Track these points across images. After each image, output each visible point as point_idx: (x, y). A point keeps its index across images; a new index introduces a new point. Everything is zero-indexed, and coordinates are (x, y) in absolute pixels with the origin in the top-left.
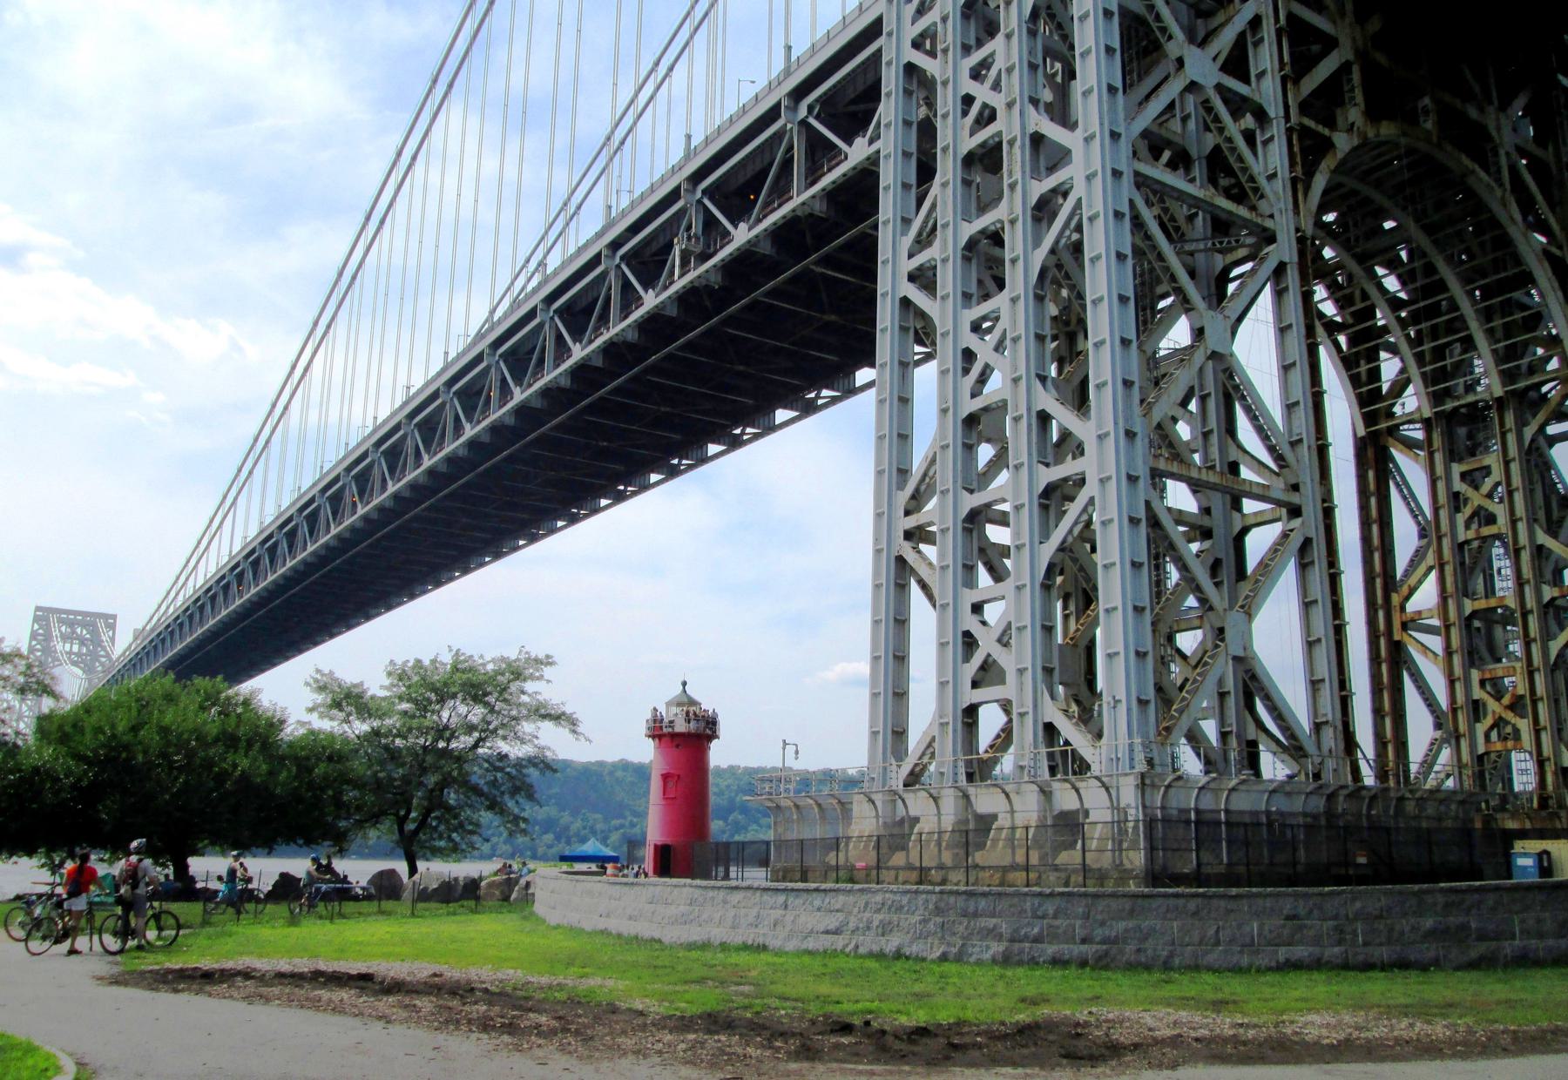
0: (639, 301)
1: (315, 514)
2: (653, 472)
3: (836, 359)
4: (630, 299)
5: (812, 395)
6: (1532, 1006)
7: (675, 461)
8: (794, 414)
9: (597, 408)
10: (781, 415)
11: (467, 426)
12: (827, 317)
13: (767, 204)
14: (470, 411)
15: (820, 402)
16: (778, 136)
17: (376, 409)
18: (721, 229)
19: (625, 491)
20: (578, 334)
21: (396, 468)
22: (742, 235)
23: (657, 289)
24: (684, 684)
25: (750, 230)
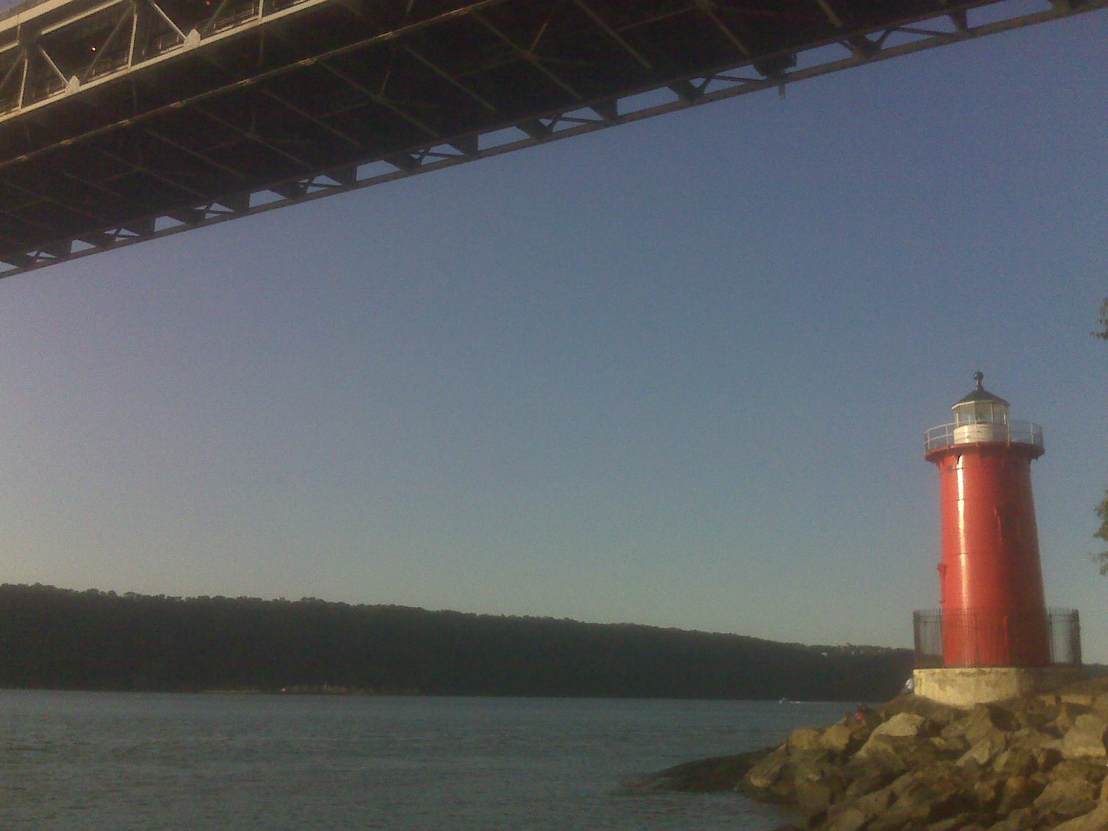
2: (258, 187)
4: (42, 83)
5: (112, 232)
10: (77, 245)
23: (205, 29)
24: (980, 376)
25: (202, 38)
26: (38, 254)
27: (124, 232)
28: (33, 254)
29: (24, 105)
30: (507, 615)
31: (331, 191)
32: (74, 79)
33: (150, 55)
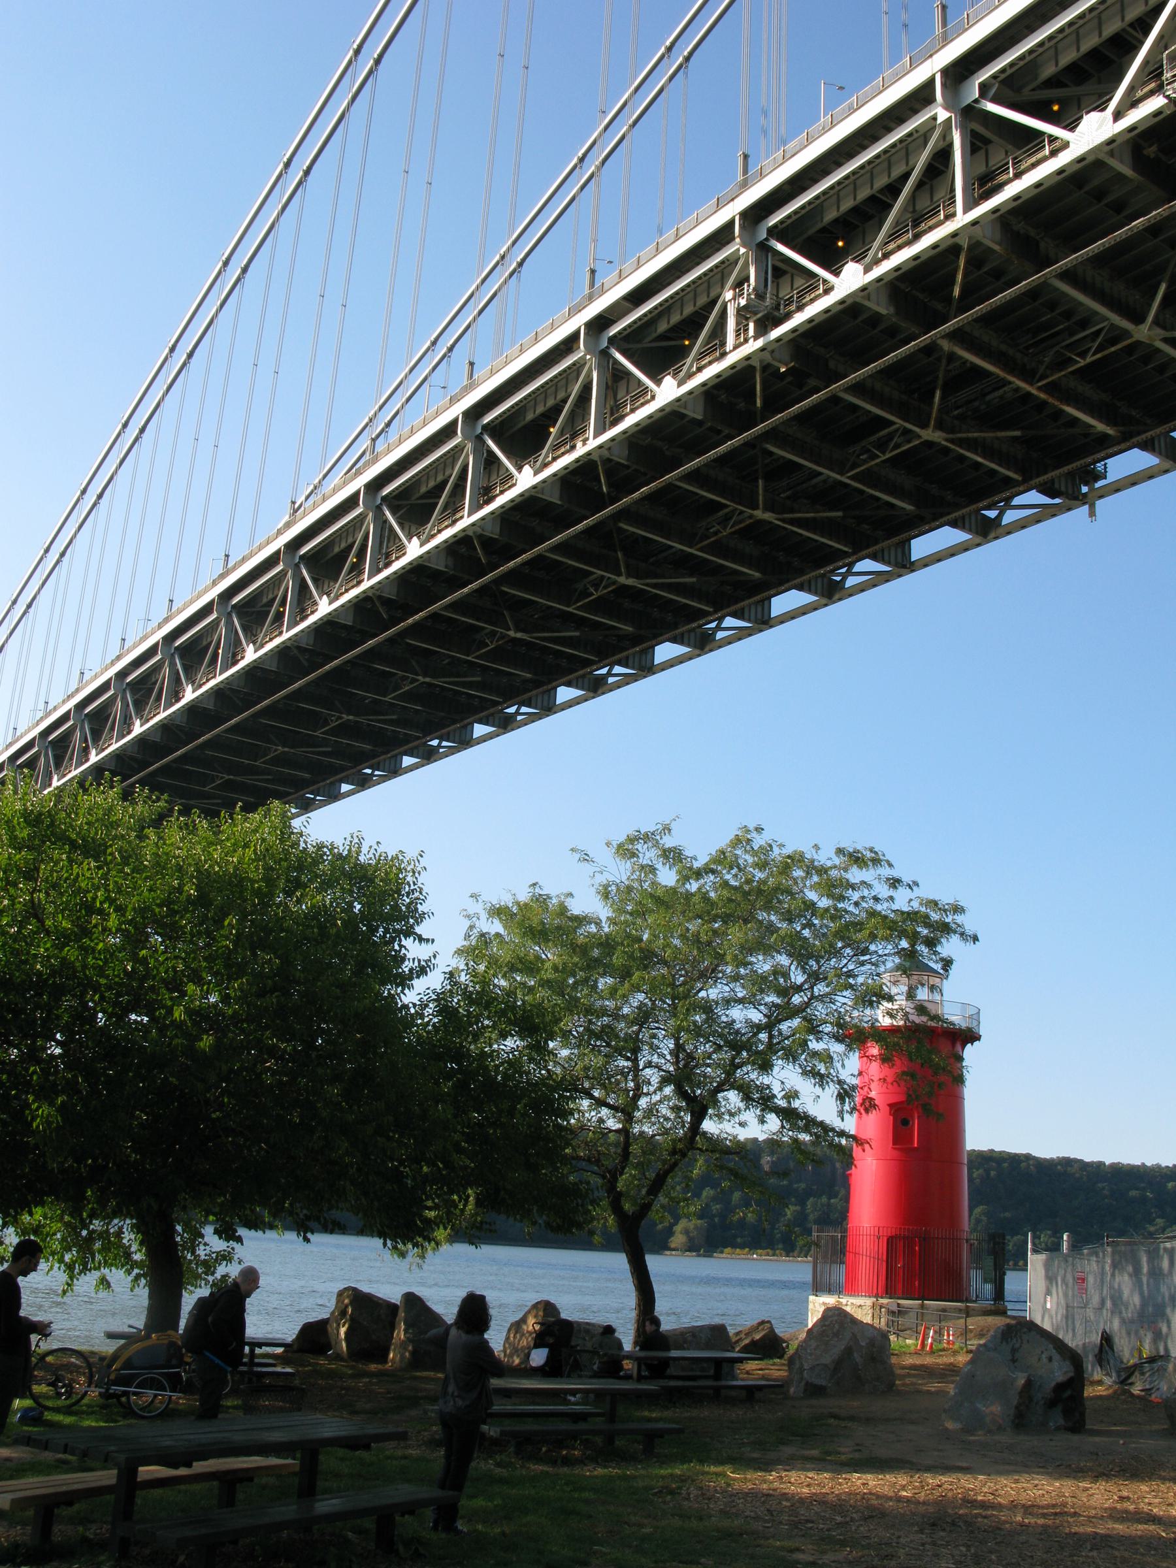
0: (401, 550)
1: (66, 738)
3: (757, 575)
4: (388, 546)
5: (604, 671)
6: (114, 1314)
7: (435, 743)
8: (579, 693)
9: (433, 628)
10: (564, 693)
11: (189, 689)
12: (622, 580)
13: (893, 236)
14: (191, 670)
15: (720, 635)
16: (577, 368)
17: (48, 693)
18: (633, 385)
19: (372, 775)
20: (252, 637)
21: (63, 758)
22: (526, 479)
23: (423, 537)
26: (518, 709)
27: (618, 669)
28: (512, 710)
29: (598, 433)
30: (1149, 1164)
31: (879, 579)
32: (527, 470)
33: (614, 423)
